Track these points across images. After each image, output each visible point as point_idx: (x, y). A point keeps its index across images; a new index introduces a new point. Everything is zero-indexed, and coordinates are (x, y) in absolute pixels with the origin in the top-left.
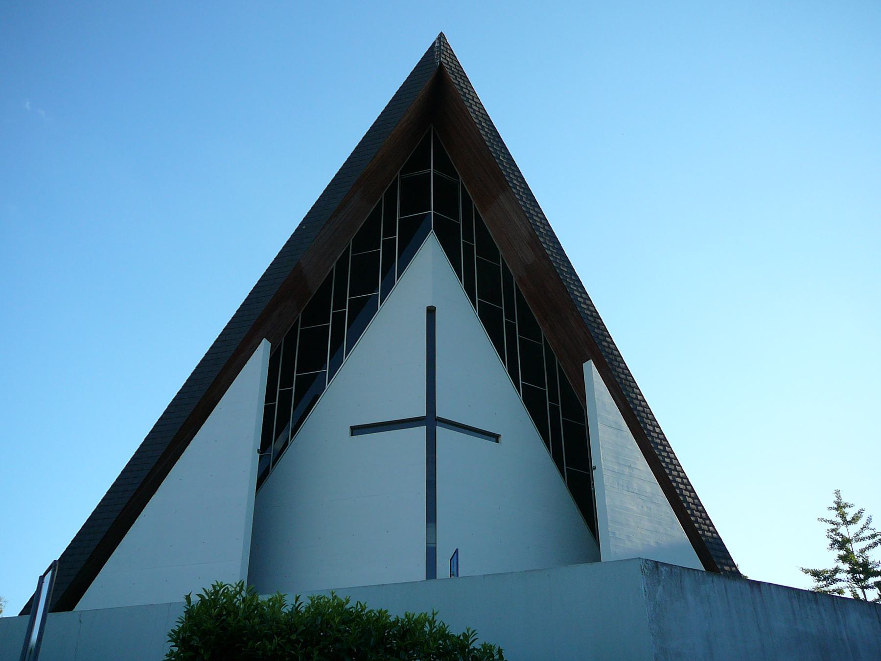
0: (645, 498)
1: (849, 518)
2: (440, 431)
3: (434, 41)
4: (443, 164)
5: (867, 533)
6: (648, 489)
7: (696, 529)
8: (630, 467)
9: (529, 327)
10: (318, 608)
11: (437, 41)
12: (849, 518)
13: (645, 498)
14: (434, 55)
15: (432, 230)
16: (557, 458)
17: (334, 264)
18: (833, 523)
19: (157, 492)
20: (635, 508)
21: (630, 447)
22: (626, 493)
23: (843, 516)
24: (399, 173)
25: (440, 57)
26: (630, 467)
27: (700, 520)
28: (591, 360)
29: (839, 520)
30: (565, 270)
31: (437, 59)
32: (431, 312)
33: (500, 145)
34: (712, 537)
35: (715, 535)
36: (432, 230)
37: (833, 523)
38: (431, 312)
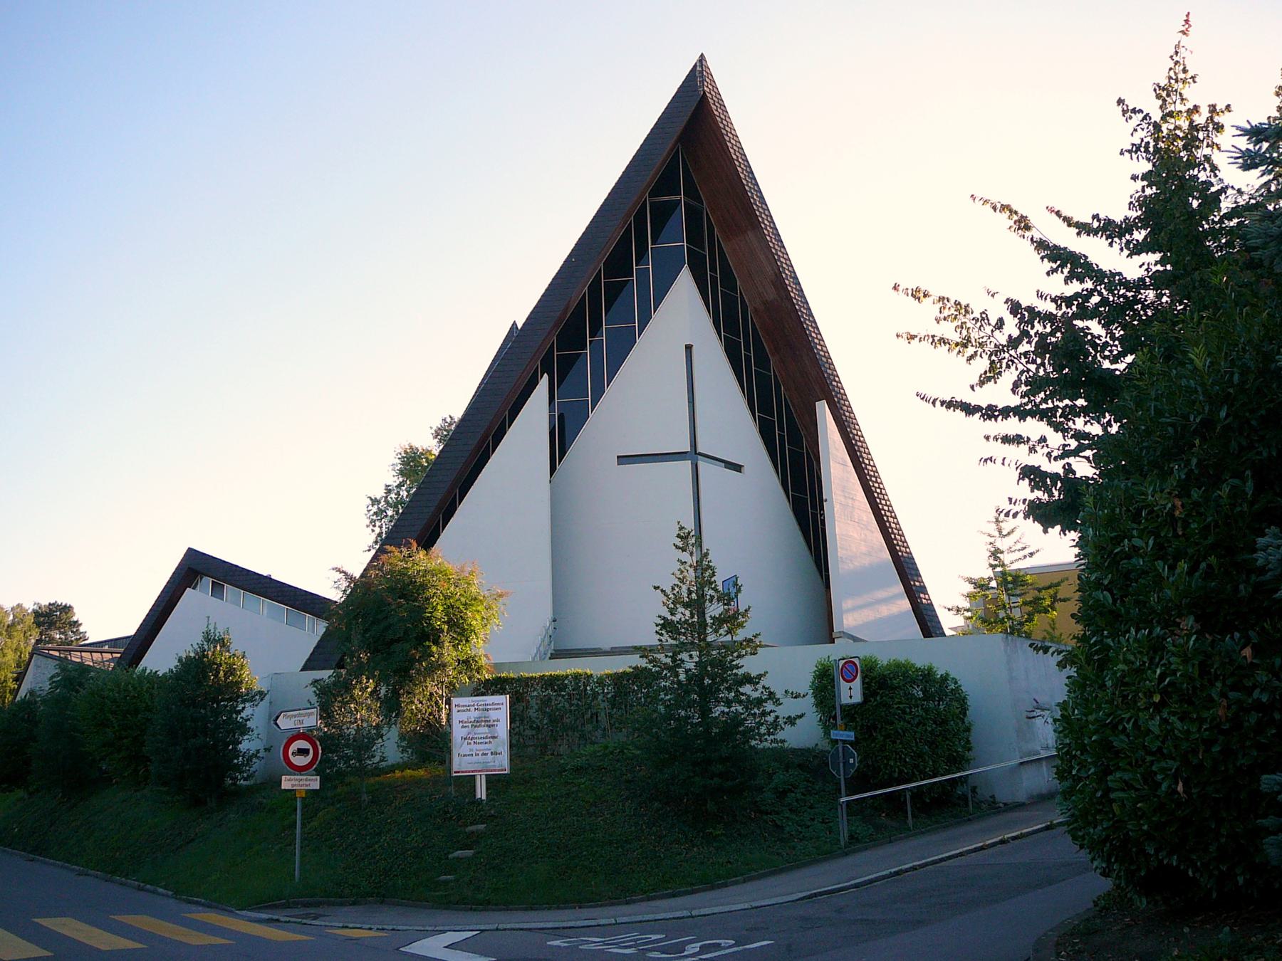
0: (862, 526)
1: (1005, 532)
2: (703, 465)
3: (694, 63)
4: (691, 192)
5: (1019, 546)
6: (865, 518)
7: (897, 551)
8: (852, 499)
9: (762, 361)
10: (889, 665)
11: (698, 64)
12: (1005, 532)
13: (862, 526)
14: (697, 82)
15: (686, 265)
16: (784, 484)
17: (586, 288)
18: (990, 536)
19: (455, 515)
20: (855, 535)
21: (853, 481)
22: (849, 522)
23: (1000, 532)
24: (647, 194)
25: (703, 85)
26: (852, 499)
27: (900, 543)
28: (825, 401)
29: (997, 534)
30: (805, 311)
31: (700, 87)
32: (689, 348)
33: (750, 176)
34: (908, 558)
35: (910, 555)
36: (686, 265)
37: (990, 536)
38: (689, 348)
